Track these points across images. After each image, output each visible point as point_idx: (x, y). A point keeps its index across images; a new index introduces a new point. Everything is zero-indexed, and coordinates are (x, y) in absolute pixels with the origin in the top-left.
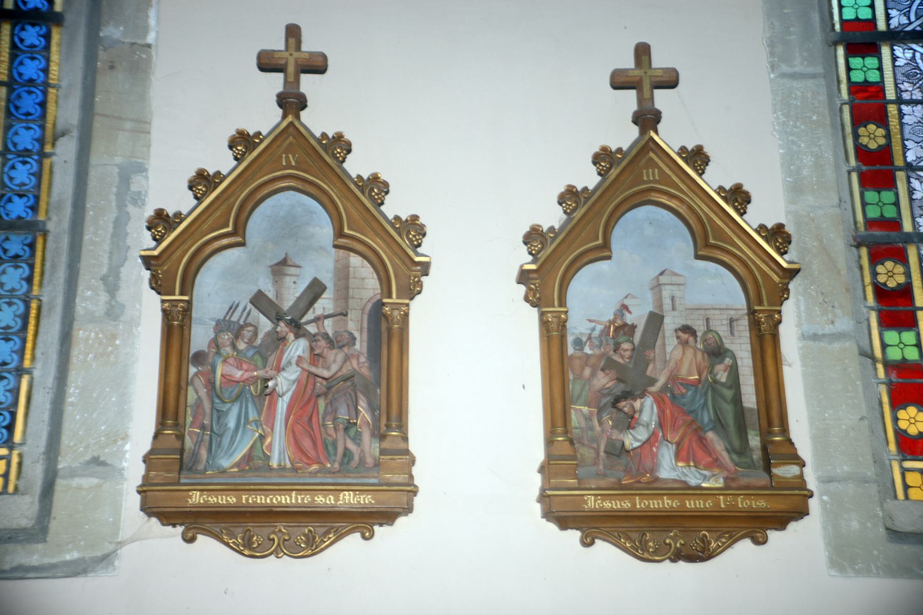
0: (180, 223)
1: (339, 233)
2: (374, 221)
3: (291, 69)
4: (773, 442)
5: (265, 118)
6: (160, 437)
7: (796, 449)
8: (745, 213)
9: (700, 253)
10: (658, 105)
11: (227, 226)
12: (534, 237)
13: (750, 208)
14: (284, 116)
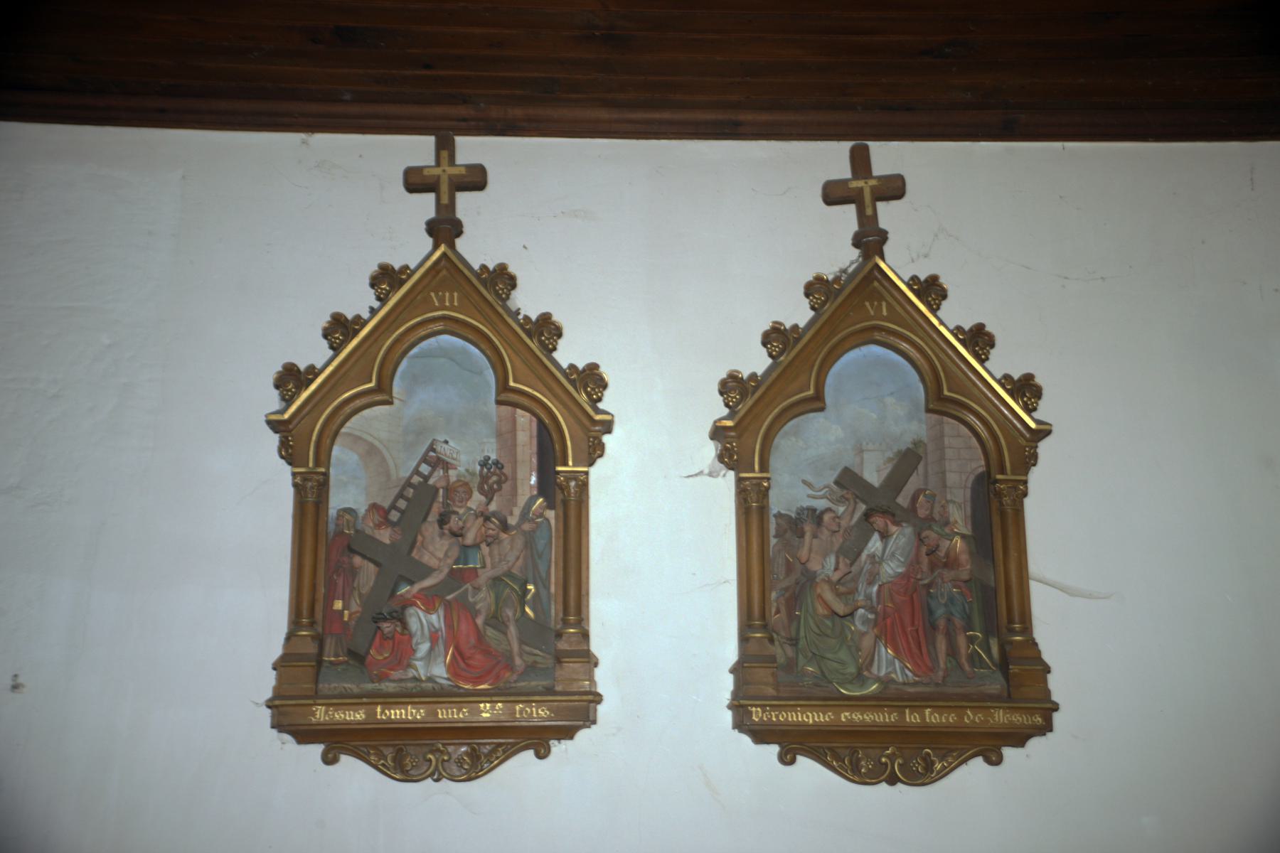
0: (311, 381)
1: (503, 386)
2: (545, 371)
3: (444, 188)
4: (1012, 643)
5: (413, 249)
6: (293, 639)
7: (1039, 652)
8: (987, 359)
9: (931, 406)
10: (883, 223)
11: (370, 381)
12: (732, 386)
13: (994, 353)
14: (436, 247)
